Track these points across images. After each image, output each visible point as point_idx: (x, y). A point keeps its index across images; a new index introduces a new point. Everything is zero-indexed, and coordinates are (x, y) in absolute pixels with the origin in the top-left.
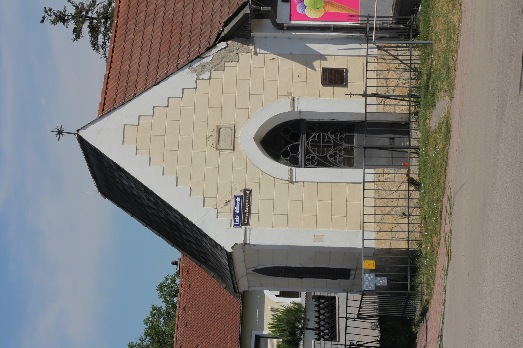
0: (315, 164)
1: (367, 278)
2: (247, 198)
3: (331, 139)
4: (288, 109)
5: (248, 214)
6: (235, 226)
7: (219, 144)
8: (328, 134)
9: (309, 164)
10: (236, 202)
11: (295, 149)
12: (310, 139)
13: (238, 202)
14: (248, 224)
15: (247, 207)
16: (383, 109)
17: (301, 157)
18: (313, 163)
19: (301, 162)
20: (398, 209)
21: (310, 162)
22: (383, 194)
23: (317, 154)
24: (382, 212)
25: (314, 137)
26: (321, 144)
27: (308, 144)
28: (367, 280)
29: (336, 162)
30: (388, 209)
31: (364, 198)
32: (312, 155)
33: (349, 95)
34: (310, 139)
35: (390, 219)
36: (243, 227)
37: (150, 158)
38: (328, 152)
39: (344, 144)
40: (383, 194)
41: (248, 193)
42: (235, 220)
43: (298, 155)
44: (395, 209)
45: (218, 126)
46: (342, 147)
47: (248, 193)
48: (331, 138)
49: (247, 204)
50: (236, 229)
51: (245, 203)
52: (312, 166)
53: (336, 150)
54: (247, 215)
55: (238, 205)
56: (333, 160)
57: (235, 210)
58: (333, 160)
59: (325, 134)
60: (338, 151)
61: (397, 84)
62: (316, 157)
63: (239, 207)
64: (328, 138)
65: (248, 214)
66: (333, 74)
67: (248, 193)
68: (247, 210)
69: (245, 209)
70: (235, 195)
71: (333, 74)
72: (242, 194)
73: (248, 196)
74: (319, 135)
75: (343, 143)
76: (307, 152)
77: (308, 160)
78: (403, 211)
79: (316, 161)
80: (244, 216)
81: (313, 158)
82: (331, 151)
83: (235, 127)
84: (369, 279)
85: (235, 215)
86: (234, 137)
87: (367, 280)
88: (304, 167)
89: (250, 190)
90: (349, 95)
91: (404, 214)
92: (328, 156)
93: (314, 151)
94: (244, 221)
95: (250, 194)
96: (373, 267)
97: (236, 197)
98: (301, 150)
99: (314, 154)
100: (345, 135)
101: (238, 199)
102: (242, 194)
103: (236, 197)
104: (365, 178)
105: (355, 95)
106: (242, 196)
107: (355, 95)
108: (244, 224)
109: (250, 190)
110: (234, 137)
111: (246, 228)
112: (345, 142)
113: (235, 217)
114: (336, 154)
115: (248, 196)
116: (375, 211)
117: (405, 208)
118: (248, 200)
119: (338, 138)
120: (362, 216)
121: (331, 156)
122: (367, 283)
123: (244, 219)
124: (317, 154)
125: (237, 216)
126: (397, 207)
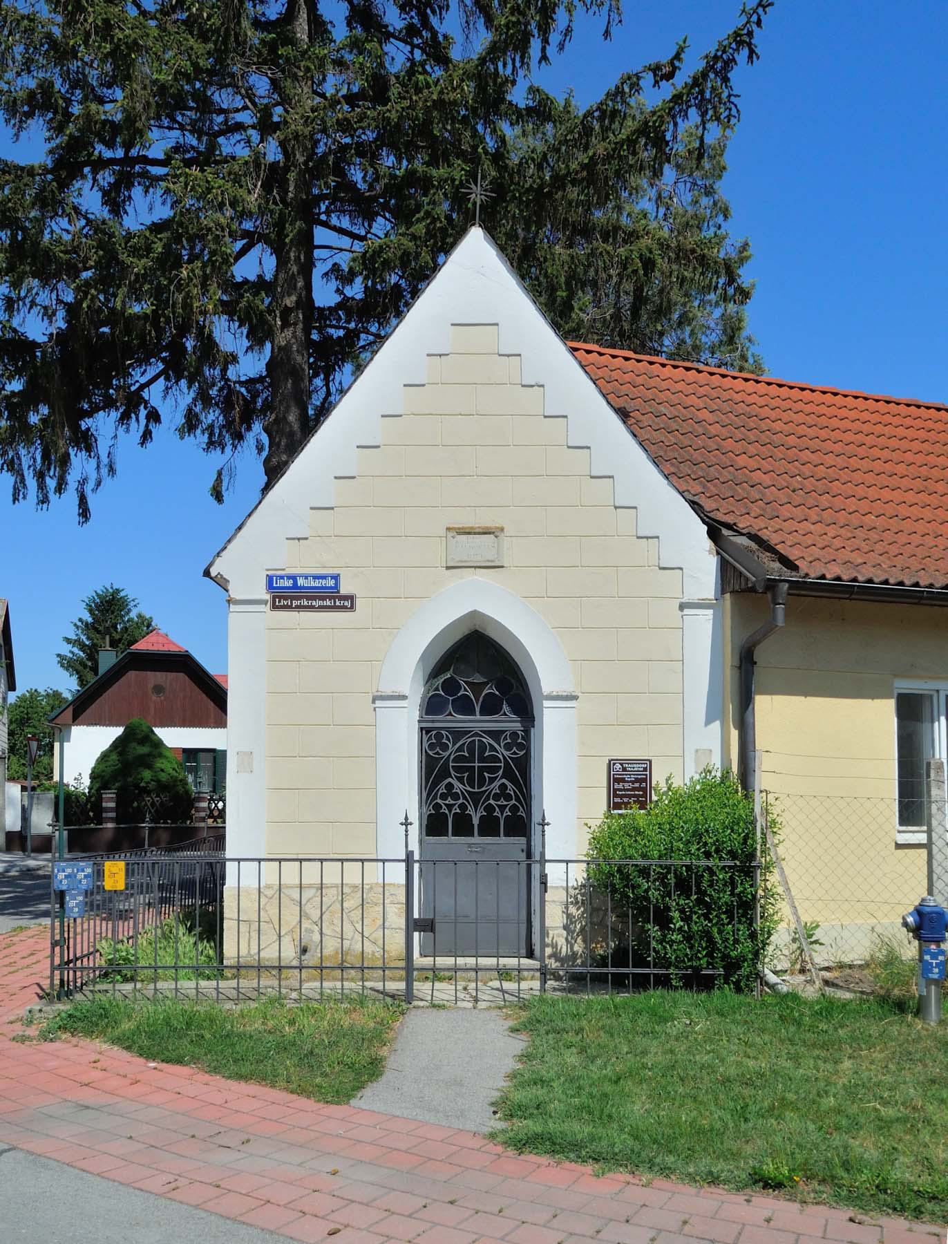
0: (431, 753)
1: (83, 871)
2: (335, 602)
3: (489, 785)
4: (547, 687)
5: (297, 607)
6: (270, 579)
7: (459, 533)
8: (501, 778)
9: (430, 739)
10: (324, 577)
11: (465, 707)
12: (487, 740)
13: (324, 582)
14: (275, 607)
15: (314, 603)
16: (554, 901)
17: (445, 721)
18: (431, 746)
19: (433, 721)
20: (316, 937)
21: (509, 741)
22: (352, 902)
23: (452, 757)
24: (308, 901)
25: (493, 748)
26: (477, 765)
27: (476, 734)
28: (78, 871)
29: (435, 798)
30: (315, 915)
31: (342, 861)
32: (450, 746)
33: (406, 818)
34: (487, 740)
35: (291, 916)
36: (268, 597)
37: (423, 385)
38: (460, 780)
39: (479, 815)
40: (352, 902)
41: (346, 604)
42: (282, 577)
43: (450, 714)
44: (317, 929)
45: (502, 530)
46: (470, 810)
47: (346, 603)
48: (492, 786)
49: (321, 603)
50: (263, 582)
51: (323, 598)
52: (426, 745)
53: (465, 798)
54: (295, 603)
55: (317, 583)
56: (440, 792)
57: (306, 578)
58: (440, 792)
59: (501, 772)
60: (461, 801)
61: (297, 943)
62: (448, 753)
63: (313, 584)
64: (492, 780)
65: (297, 607)
66: (637, 785)
67: (346, 603)
68: (306, 603)
69: (308, 598)
70: (339, 575)
71: (637, 785)
72: (344, 591)
73: (338, 603)
74: (496, 759)
75: (481, 812)
76: (457, 734)
77: (439, 736)
78: (312, 947)
79: (437, 753)
80: (293, 598)
81: (445, 747)
82: (461, 786)
83: (502, 567)
84: (81, 875)
85: (293, 578)
86: (475, 567)
87: (78, 871)
88: (422, 729)
89: (352, 608)
90: (406, 818)
91: (304, 951)
92: (450, 780)
93: (460, 749)
94: (280, 598)
95: (343, 608)
96: (108, 885)
97: (336, 578)
98: (460, 721)
99: (452, 748)
100: (499, 815)
101: (331, 583)
102: (344, 591)
103: (336, 578)
104: (267, 863)
105: (406, 835)
106: (338, 592)
107: (406, 835)
108: (274, 598)
109: (352, 608)
110: (475, 567)
111: (265, 602)
112: (482, 817)
113: (289, 577)
114: (456, 797)
115: (338, 603)
116: (310, 886)
117: (319, 951)
118: (329, 603)
119: (492, 802)
120: (300, 857)
121: (449, 786)
122: (69, 871)
123: (286, 598)
124: (452, 757)
125: (291, 582)
126: (321, 934)
